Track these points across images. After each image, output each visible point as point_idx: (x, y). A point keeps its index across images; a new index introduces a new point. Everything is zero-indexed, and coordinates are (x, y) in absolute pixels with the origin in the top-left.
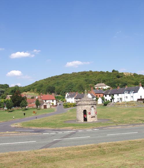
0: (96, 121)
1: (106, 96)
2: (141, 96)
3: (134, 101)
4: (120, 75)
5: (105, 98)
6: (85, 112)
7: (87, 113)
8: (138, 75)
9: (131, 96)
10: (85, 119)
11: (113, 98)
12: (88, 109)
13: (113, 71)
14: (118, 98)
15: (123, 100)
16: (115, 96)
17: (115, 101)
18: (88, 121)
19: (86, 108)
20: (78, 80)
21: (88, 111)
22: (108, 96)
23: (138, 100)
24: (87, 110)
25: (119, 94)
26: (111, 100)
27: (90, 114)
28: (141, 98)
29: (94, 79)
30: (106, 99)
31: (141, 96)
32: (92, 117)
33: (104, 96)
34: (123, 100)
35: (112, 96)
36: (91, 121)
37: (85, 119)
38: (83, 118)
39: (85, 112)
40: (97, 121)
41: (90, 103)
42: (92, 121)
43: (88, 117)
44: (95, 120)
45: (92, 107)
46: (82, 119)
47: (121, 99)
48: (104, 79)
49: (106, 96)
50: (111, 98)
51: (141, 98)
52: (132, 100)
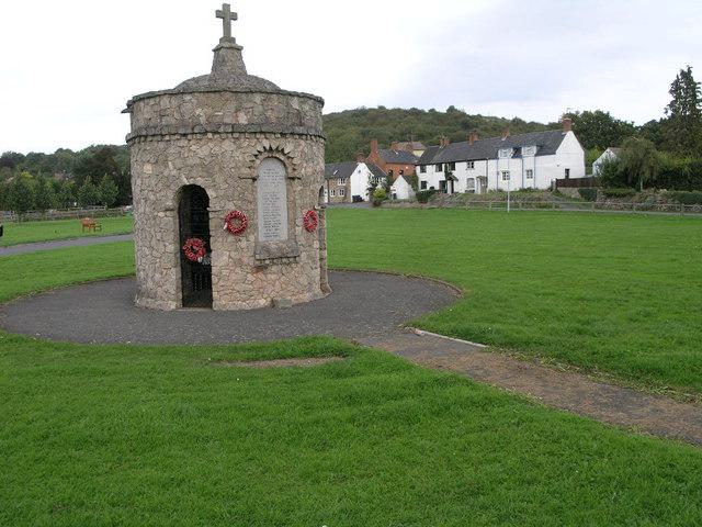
0: (306, 297)
1: (423, 171)
2: (567, 170)
3: (536, 190)
4: (474, 122)
5: (422, 177)
6: (193, 206)
7: (216, 223)
8: (524, 122)
9: (527, 167)
10: (197, 282)
11: (450, 178)
12: (219, 178)
13: (451, 109)
14: (468, 180)
15: (492, 185)
16: (461, 170)
17: (461, 187)
18: (221, 299)
19: (202, 165)
20: (340, 131)
21: (220, 205)
22: (430, 169)
23: (559, 183)
24: (211, 193)
25: (475, 163)
26: (443, 184)
27: (238, 225)
28: (567, 176)
29: (387, 130)
30: (424, 184)
31: (567, 170)
32: (260, 268)
33: (418, 168)
34: (492, 185)
35: (446, 167)
36: (246, 306)
37: (197, 282)
38: (174, 275)
39: (193, 206)
40: (313, 303)
41: (243, 119)
42: (263, 302)
43: (224, 257)
44: (301, 284)
45: (272, 154)
46: (162, 280)
47: (484, 180)
48: (419, 130)
49: (423, 171)
50: (441, 176)
51: (567, 176)
52: (529, 183)
